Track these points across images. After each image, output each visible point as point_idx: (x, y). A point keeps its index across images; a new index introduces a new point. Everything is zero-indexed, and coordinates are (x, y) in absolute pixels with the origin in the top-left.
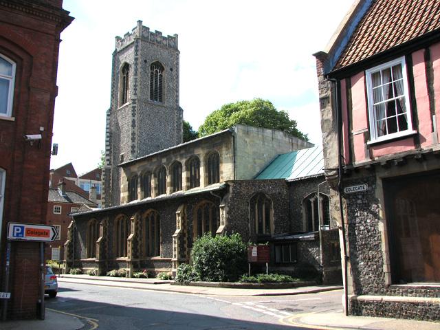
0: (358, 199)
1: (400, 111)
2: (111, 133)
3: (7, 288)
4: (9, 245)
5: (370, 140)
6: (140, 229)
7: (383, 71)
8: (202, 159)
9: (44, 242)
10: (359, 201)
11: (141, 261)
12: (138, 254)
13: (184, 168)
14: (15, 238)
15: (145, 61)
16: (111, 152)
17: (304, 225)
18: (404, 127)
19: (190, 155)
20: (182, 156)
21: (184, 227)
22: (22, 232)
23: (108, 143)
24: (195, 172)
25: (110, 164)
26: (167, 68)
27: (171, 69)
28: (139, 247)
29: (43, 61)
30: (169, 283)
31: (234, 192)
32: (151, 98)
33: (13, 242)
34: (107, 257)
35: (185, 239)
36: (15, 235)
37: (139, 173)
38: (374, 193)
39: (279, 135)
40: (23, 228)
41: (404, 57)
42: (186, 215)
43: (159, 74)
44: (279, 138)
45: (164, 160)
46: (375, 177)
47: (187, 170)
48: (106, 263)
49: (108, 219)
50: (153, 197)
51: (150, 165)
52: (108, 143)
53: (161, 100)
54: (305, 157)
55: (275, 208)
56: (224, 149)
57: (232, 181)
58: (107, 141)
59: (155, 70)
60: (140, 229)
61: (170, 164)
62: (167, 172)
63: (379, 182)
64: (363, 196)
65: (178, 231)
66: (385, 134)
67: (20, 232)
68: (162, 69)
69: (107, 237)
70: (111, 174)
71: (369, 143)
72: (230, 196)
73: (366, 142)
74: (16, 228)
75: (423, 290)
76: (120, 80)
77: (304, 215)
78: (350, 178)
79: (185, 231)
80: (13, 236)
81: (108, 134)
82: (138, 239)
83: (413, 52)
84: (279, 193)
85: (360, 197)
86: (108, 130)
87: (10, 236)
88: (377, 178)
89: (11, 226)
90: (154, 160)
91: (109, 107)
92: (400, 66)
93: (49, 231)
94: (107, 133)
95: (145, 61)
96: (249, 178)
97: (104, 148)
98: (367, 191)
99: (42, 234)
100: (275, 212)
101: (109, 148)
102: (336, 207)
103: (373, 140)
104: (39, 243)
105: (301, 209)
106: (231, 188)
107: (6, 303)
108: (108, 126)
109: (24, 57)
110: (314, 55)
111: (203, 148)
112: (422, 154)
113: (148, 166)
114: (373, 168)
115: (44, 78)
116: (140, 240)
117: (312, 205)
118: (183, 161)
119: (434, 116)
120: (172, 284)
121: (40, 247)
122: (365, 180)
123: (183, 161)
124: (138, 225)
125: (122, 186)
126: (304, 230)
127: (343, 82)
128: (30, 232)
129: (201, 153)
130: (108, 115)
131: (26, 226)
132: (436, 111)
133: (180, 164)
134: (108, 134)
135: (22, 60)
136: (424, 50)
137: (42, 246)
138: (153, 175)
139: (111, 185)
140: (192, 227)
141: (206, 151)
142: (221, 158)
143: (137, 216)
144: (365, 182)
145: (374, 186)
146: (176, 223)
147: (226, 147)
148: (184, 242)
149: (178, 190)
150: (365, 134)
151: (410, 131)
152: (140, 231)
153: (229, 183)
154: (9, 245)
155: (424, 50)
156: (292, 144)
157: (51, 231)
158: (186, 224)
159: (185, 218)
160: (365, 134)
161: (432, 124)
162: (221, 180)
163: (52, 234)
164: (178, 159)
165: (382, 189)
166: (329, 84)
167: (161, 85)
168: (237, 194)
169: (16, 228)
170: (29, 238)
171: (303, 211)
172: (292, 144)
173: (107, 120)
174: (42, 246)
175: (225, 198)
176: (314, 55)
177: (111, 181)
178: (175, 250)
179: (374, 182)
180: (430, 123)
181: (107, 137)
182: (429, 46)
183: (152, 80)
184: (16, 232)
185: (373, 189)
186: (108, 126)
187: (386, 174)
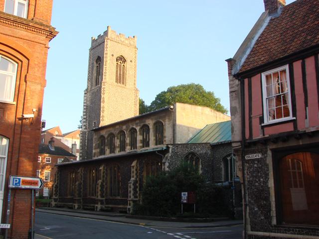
0: (255, 163)
1: (285, 102)
2: (87, 106)
3: (8, 221)
4: (10, 191)
5: (263, 123)
6: (105, 176)
7: (274, 74)
8: (151, 127)
9: (35, 190)
10: (255, 165)
11: (106, 199)
12: (104, 194)
13: (138, 133)
14: (14, 186)
15: (113, 55)
16: (87, 120)
17: (223, 177)
18: (287, 115)
19: (142, 124)
20: (137, 125)
21: (137, 176)
22: (19, 182)
23: (85, 114)
24: (146, 137)
25: (86, 129)
26: (128, 61)
27: (131, 61)
28: (104, 189)
29: (36, 63)
30: (124, 216)
31: (172, 152)
32: (117, 82)
33: (13, 189)
34: (82, 196)
35: (138, 185)
36: (14, 184)
37: (106, 136)
38: (266, 160)
39: (207, 110)
40: (19, 179)
41: (288, 65)
42: (139, 168)
43: (122, 64)
44: (207, 112)
45: (124, 127)
46: (267, 148)
47: (140, 134)
48: (82, 201)
49: (83, 169)
50: (117, 153)
51: (115, 130)
52: (85, 114)
53: (123, 83)
54: (214, 138)
55: (202, 164)
56: (167, 120)
57: (172, 145)
58: (84, 112)
59: (119, 61)
60: (105, 176)
61: (128, 130)
62: (126, 136)
63: (270, 153)
64: (258, 162)
65: (132, 179)
66: (275, 119)
67: (17, 182)
68: (125, 61)
69: (82, 182)
70: (87, 136)
71: (262, 125)
72: (170, 155)
73: (260, 124)
74: (15, 179)
75: (297, 230)
76: (95, 68)
77: (223, 169)
78: (250, 149)
79: (138, 179)
80: (13, 185)
81: (85, 107)
82: (104, 184)
83: (294, 62)
84: (205, 153)
85: (256, 162)
86: (85, 104)
87: (11, 186)
88: (268, 149)
89: (12, 178)
90: (117, 127)
91: (86, 87)
92: (284, 71)
93: (38, 181)
94: (84, 106)
95: (113, 55)
96: (184, 142)
97: (82, 114)
98: (261, 158)
99: (33, 183)
100: (202, 166)
101: (85, 117)
102: (239, 169)
103: (266, 122)
104: (30, 190)
105: (221, 165)
106: (170, 150)
107: (7, 232)
108: (85, 102)
109: (20, 63)
110: (226, 60)
111: (152, 119)
112: (299, 134)
113: (113, 132)
114: (265, 142)
115: (36, 75)
116: (106, 184)
117: (229, 162)
118: (138, 129)
119: (307, 108)
120: (127, 217)
121: (31, 193)
122: (260, 150)
123: (138, 129)
124: (105, 174)
125: (94, 145)
126: (223, 180)
127: (246, 81)
128: (25, 182)
129: (150, 123)
130: (85, 94)
131: (22, 178)
132: (308, 104)
133: (136, 130)
134: (85, 107)
135: (22, 62)
136: (301, 61)
137: (33, 191)
138: (116, 138)
139: (86, 144)
140: (142, 176)
141: (154, 121)
142: (164, 127)
143: (104, 167)
144: (259, 152)
145: (266, 155)
146: (131, 173)
147: (169, 119)
148: (137, 187)
149: (134, 149)
150: (260, 118)
151: (291, 118)
152: (106, 178)
153: (169, 146)
154: (10, 191)
155: (301, 61)
156: (216, 117)
157: (40, 181)
158: (138, 174)
159: (138, 170)
160: (260, 118)
161: (306, 113)
162: (164, 143)
163: (40, 184)
164: (134, 127)
165: (271, 158)
166: (237, 82)
167: (123, 73)
168: (175, 154)
169: (15, 179)
170: (23, 187)
171: (222, 166)
172: (216, 117)
173: (84, 96)
174: (33, 191)
175: (166, 155)
176: (226, 60)
177: (86, 141)
178: (130, 191)
179: (266, 152)
180: (305, 112)
181: (84, 109)
182: (306, 58)
183: (117, 68)
184: (15, 182)
185: (265, 157)
186: (85, 102)
187: (274, 147)
